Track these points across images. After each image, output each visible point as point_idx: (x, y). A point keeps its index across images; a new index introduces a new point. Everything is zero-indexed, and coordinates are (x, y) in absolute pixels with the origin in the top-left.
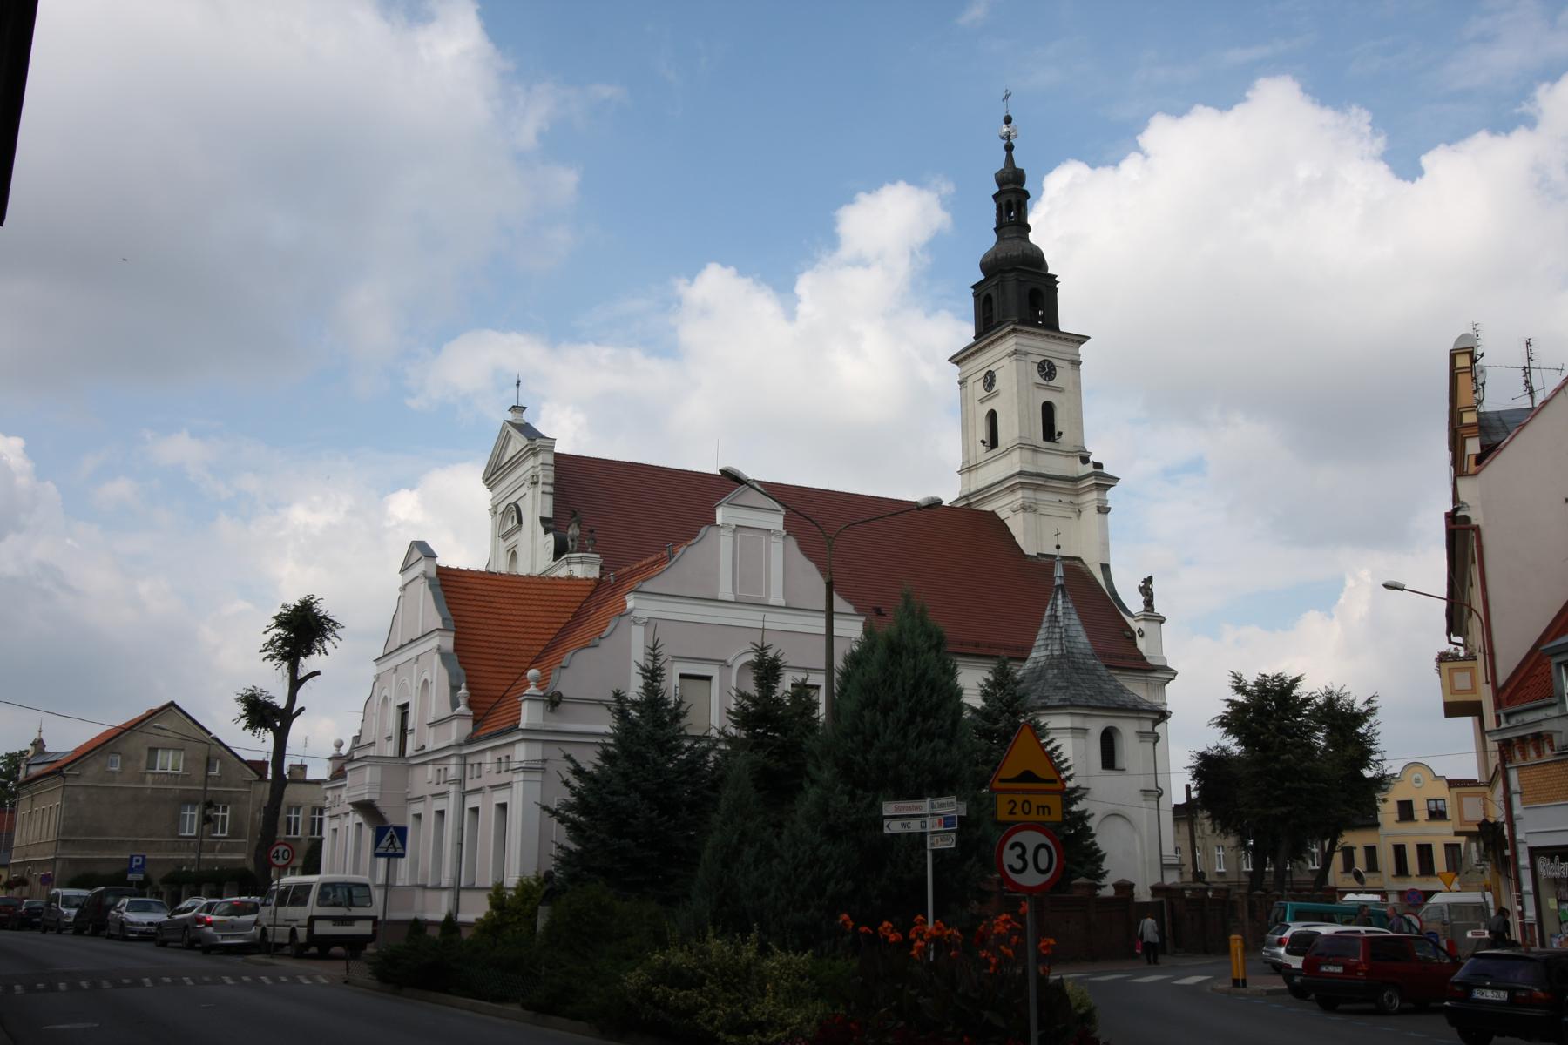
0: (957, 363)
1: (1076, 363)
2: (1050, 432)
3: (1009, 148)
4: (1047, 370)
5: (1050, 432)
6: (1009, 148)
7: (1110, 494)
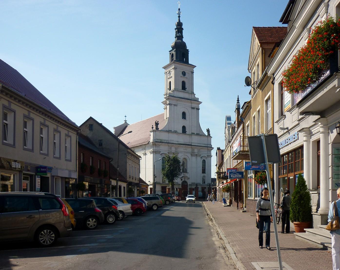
0: (164, 69)
1: (193, 73)
2: (184, 88)
3: (179, 17)
4: (184, 74)
5: (184, 88)
6: (179, 17)
7: (195, 69)
